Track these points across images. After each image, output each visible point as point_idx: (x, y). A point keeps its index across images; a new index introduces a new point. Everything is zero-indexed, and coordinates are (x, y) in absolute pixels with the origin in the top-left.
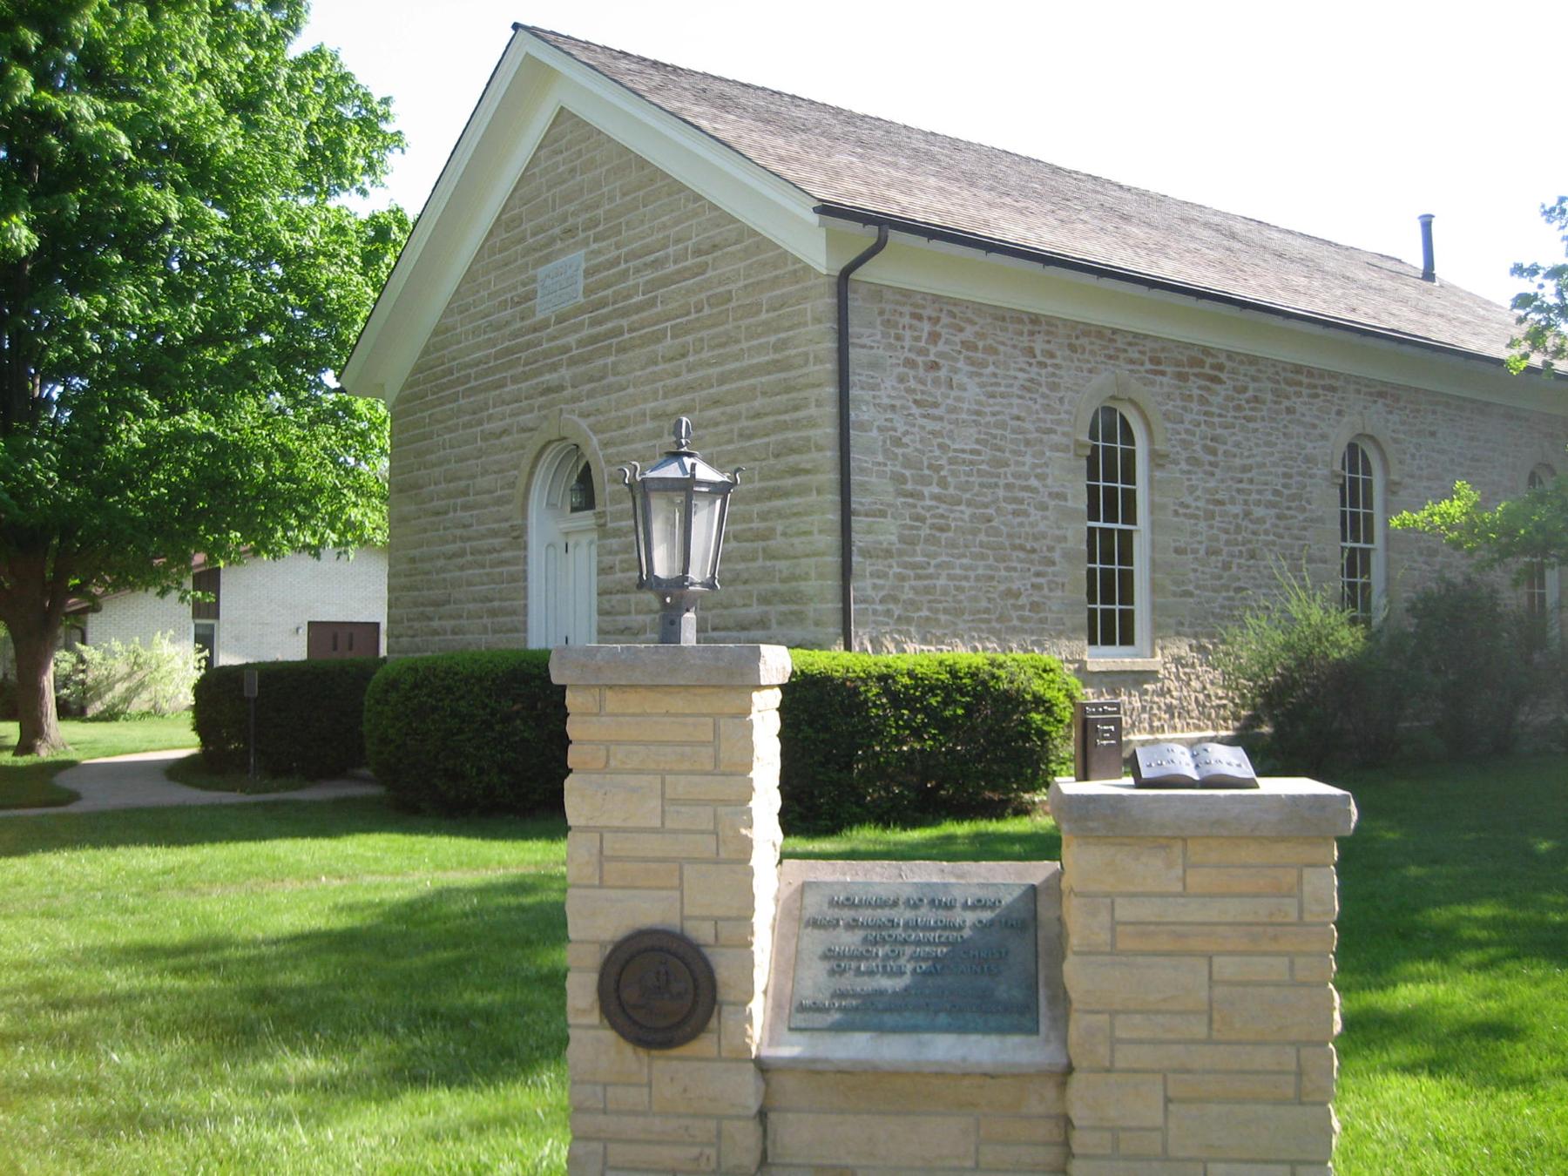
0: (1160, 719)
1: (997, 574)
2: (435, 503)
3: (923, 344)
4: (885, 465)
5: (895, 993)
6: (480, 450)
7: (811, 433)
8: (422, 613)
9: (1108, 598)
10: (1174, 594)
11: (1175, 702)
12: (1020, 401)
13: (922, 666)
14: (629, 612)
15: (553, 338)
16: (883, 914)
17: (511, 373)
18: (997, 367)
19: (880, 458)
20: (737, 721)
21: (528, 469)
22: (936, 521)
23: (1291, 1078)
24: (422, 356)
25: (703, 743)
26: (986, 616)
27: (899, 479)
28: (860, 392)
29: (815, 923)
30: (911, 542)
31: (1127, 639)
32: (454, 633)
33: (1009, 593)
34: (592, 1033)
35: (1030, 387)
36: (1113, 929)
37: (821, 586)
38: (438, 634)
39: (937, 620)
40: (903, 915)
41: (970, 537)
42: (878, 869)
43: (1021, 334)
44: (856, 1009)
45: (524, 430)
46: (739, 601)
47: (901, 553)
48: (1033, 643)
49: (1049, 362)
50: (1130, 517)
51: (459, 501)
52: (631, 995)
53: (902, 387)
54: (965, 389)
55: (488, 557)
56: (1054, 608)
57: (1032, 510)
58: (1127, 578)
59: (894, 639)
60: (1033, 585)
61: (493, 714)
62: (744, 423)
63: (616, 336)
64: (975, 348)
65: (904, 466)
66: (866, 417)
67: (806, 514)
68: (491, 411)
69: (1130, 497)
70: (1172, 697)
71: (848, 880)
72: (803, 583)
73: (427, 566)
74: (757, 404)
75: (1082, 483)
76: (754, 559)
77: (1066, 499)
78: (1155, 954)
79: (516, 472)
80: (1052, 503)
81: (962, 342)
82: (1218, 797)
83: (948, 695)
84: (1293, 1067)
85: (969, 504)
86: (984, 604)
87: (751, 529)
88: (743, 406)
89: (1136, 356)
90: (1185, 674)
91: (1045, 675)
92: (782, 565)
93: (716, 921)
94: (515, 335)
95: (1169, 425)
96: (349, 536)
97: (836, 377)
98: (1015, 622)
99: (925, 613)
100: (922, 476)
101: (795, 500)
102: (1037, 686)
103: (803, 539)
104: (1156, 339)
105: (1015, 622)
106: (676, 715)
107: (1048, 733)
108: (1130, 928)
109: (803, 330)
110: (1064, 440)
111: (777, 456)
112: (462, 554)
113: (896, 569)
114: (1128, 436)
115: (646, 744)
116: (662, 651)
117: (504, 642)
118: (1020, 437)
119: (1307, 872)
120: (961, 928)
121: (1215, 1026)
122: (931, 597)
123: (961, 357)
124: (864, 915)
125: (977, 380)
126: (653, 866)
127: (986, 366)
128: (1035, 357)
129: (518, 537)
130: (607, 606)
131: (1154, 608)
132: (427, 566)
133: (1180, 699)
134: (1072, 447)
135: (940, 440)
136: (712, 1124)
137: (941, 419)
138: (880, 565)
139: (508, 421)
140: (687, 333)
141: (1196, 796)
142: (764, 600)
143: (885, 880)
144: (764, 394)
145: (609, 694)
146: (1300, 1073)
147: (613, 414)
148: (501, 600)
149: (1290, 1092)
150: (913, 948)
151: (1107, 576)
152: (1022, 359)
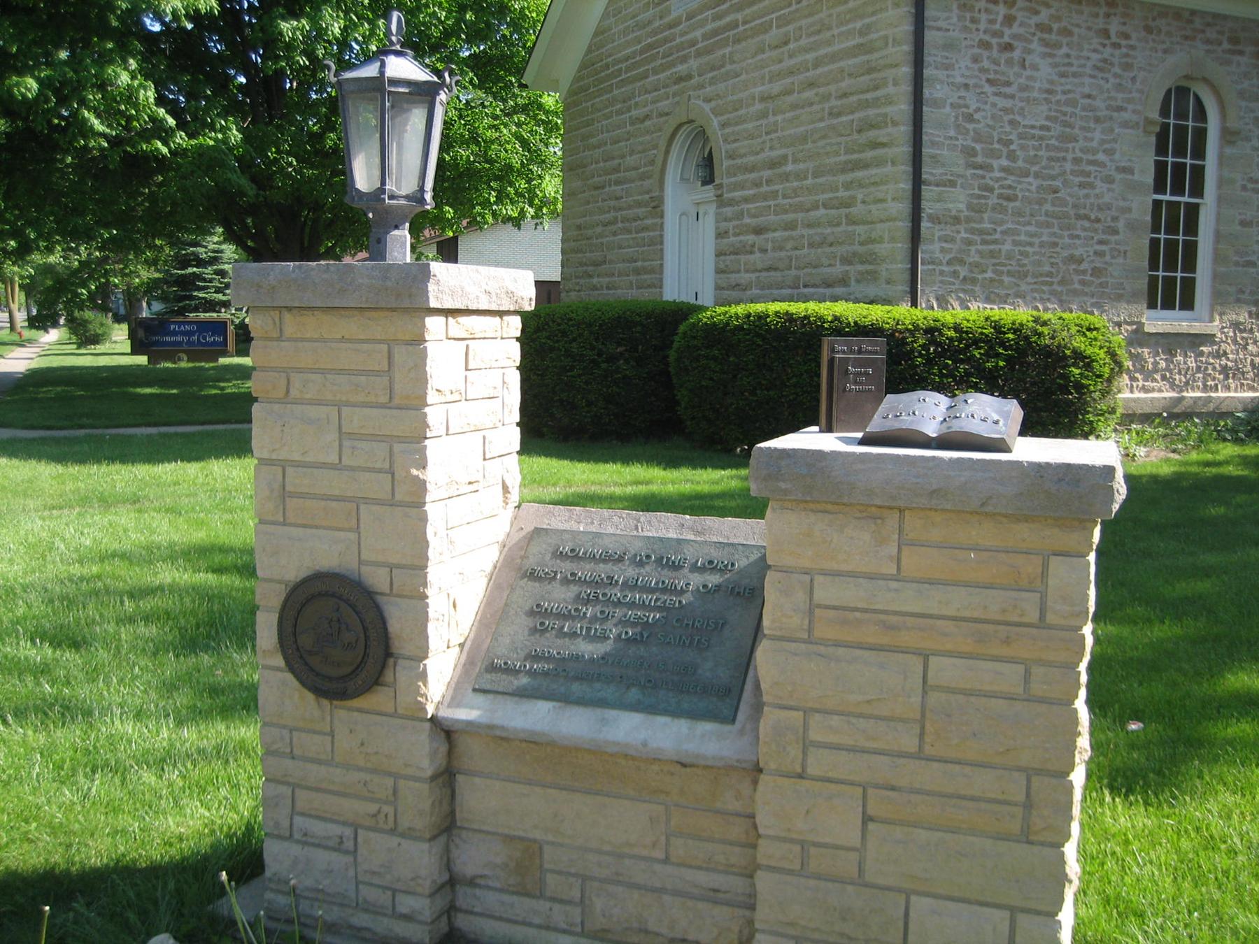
0: (1214, 379)
1: (1060, 241)
2: (596, 179)
3: (997, 26)
4: (957, 139)
5: (592, 660)
6: (629, 133)
7: (888, 109)
8: (586, 272)
9: (1171, 265)
10: (1237, 264)
11: (1230, 364)
12: (1092, 80)
13: (968, 321)
14: (739, 271)
15: (683, 34)
16: (603, 570)
17: (653, 65)
18: (1071, 49)
19: (952, 133)
20: (410, 348)
21: (664, 148)
22: (1002, 191)
23: (1018, 811)
24: (586, 55)
25: (377, 373)
26: (1048, 279)
27: (970, 152)
28: (935, 72)
29: (532, 575)
30: (980, 210)
31: (1188, 304)
32: (608, 288)
33: (1072, 259)
34: (280, 675)
35: (1103, 67)
36: (811, 612)
37: (893, 249)
38: (597, 289)
39: (1001, 282)
40: (626, 572)
41: (1037, 207)
42: (615, 519)
43: (1097, 15)
44: (546, 674)
45: (661, 115)
46: (825, 261)
47: (968, 220)
48: (1093, 305)
49: (1124, 42)
50: (1198, 190)
51: (613, 177)
52: (306, 641)
53: (976, 66)
54: (1038, 70)
55: (634, 224)
56: (1115, 274)
57: (1098, 183)
58: (1191, 249)
59: (959, 298)
60: (1096, 253)
61: (599, 355)
62: (834, 102)
63: (733, 29)
64: (1050, 30)
65: (975, 140)
66: (940, 95)
67: (882, 183)
68: (637, 99)
69: (1199, 173)
70: (1228, 359)
71: (582, 529)
72: (878, 246)
73: (590, 232)
74: (843, 85)
75: (1150, 159)
76: (838, 224)
77: (1133, 174)
78: (860, 646)
79: (655, 152)
80: (1118, 177)
81: (1037, 25)
82: (941, 459)
83: (991, 348)
84: (1021, 797)
85: (1037, 175)
86: (1047, 268)
87: (837, 198)
88: (832, 88)
89: (1214, 36)
90: (1242, 338)
91: (1087, 333)
92: (860, 229)
93: (391, 567)
94: (655, 33)
95: (1243, 104)
96: (545, 210)
97: (911, 58)
98: (1077, 286)
99: (989, 275)
100: (992, 150)
101: (874, 171)
102: (1079, 343)
103: (879, 206)
104: (1236, 19)
105: (1077, 286)
106: (350, 341)
107: (1083, 386)
108: (831, 613)
109: (884, 15)
110: (1135, 118)
111: (859, 131)
112: (614, 222)
113: (964, 235)
114: (1201, 114)
115: (323, 372)
116: (332, 269)
117: (645, 295)
118: (1090, 114)
119: (1054, 560)
120: (682, 592)
121: (928, 739)
122: (994, 261)
123: (1036, 38)
124: (585, 570)
125: (1050, 60)
126: (334, 504)
127: (1061, 47)
128: (1109, 37)
129: (657, 207)
130: (722, 266)
131: (1215, 276)
132: (590, 232)
133: (1236, 361)
134: (1142, 123)
135: (1011, 117)
136: (389, 782)
137: (1012, 97)
138: (949, 230)
139: (649, 107)
140: (788, 23)
141: (984, 461)
142: (846, 261)
143: (618, 532)
144: (850, 75)
145: (287, 317)
146: (1028, 805)
147: (730, 98)
148: (644, 260)
149: (1015, 827)
150: (625, 610)
151: (1171, 246)
152: (1095, 40)
